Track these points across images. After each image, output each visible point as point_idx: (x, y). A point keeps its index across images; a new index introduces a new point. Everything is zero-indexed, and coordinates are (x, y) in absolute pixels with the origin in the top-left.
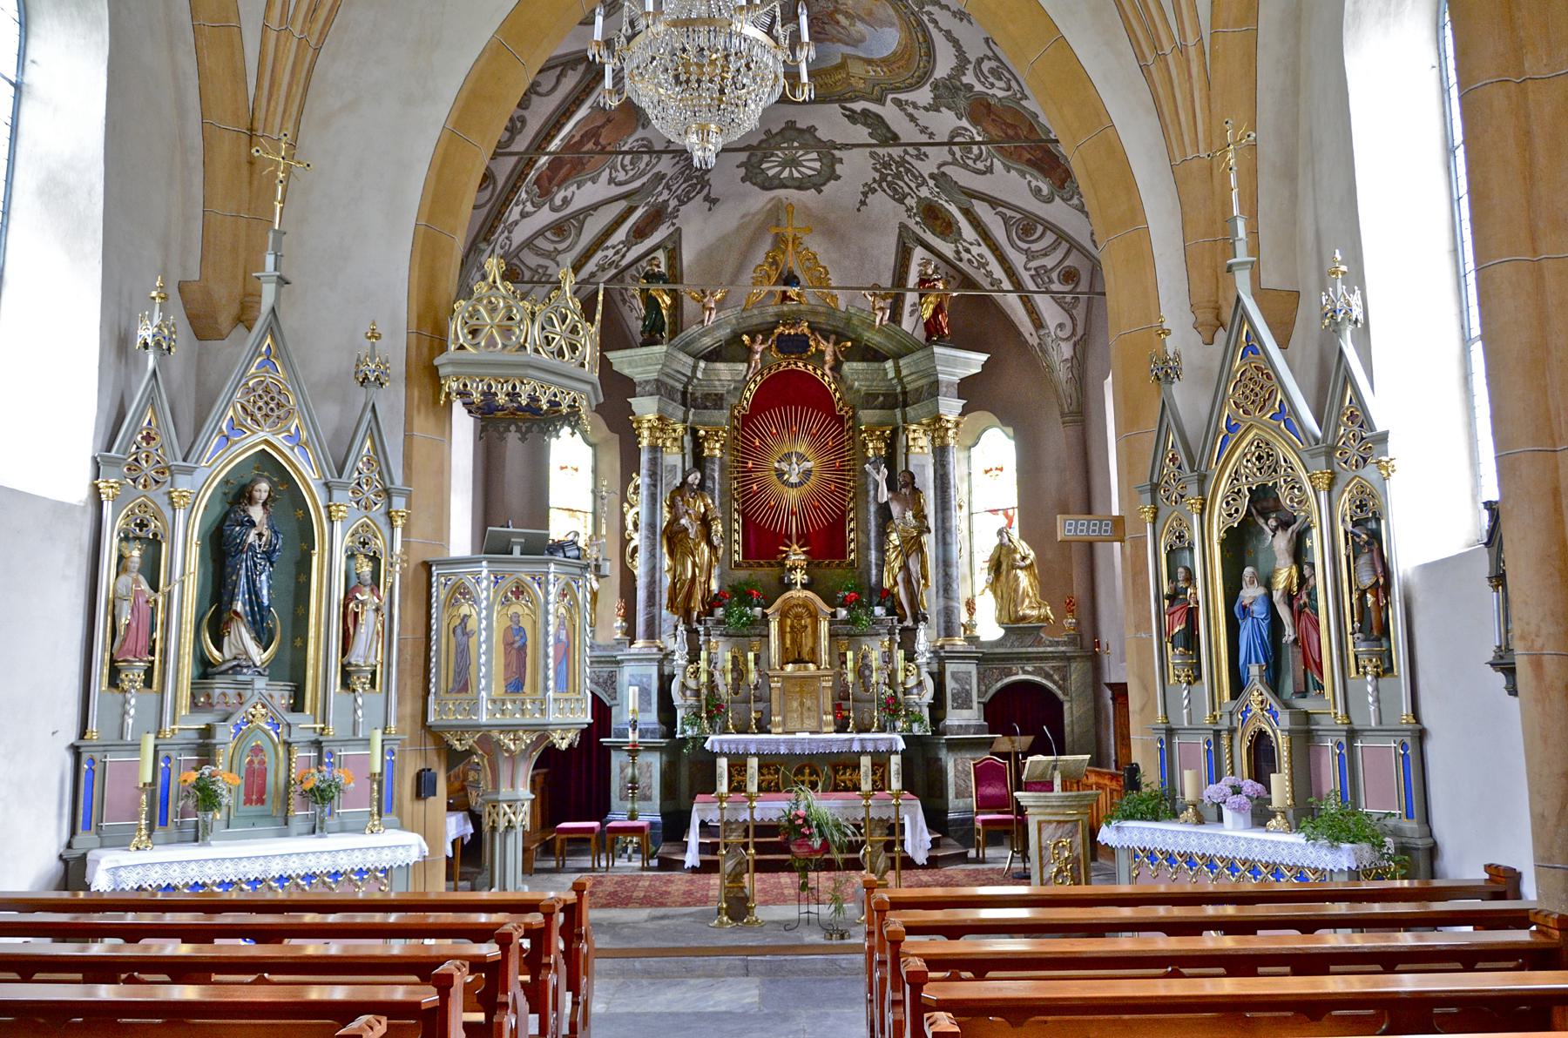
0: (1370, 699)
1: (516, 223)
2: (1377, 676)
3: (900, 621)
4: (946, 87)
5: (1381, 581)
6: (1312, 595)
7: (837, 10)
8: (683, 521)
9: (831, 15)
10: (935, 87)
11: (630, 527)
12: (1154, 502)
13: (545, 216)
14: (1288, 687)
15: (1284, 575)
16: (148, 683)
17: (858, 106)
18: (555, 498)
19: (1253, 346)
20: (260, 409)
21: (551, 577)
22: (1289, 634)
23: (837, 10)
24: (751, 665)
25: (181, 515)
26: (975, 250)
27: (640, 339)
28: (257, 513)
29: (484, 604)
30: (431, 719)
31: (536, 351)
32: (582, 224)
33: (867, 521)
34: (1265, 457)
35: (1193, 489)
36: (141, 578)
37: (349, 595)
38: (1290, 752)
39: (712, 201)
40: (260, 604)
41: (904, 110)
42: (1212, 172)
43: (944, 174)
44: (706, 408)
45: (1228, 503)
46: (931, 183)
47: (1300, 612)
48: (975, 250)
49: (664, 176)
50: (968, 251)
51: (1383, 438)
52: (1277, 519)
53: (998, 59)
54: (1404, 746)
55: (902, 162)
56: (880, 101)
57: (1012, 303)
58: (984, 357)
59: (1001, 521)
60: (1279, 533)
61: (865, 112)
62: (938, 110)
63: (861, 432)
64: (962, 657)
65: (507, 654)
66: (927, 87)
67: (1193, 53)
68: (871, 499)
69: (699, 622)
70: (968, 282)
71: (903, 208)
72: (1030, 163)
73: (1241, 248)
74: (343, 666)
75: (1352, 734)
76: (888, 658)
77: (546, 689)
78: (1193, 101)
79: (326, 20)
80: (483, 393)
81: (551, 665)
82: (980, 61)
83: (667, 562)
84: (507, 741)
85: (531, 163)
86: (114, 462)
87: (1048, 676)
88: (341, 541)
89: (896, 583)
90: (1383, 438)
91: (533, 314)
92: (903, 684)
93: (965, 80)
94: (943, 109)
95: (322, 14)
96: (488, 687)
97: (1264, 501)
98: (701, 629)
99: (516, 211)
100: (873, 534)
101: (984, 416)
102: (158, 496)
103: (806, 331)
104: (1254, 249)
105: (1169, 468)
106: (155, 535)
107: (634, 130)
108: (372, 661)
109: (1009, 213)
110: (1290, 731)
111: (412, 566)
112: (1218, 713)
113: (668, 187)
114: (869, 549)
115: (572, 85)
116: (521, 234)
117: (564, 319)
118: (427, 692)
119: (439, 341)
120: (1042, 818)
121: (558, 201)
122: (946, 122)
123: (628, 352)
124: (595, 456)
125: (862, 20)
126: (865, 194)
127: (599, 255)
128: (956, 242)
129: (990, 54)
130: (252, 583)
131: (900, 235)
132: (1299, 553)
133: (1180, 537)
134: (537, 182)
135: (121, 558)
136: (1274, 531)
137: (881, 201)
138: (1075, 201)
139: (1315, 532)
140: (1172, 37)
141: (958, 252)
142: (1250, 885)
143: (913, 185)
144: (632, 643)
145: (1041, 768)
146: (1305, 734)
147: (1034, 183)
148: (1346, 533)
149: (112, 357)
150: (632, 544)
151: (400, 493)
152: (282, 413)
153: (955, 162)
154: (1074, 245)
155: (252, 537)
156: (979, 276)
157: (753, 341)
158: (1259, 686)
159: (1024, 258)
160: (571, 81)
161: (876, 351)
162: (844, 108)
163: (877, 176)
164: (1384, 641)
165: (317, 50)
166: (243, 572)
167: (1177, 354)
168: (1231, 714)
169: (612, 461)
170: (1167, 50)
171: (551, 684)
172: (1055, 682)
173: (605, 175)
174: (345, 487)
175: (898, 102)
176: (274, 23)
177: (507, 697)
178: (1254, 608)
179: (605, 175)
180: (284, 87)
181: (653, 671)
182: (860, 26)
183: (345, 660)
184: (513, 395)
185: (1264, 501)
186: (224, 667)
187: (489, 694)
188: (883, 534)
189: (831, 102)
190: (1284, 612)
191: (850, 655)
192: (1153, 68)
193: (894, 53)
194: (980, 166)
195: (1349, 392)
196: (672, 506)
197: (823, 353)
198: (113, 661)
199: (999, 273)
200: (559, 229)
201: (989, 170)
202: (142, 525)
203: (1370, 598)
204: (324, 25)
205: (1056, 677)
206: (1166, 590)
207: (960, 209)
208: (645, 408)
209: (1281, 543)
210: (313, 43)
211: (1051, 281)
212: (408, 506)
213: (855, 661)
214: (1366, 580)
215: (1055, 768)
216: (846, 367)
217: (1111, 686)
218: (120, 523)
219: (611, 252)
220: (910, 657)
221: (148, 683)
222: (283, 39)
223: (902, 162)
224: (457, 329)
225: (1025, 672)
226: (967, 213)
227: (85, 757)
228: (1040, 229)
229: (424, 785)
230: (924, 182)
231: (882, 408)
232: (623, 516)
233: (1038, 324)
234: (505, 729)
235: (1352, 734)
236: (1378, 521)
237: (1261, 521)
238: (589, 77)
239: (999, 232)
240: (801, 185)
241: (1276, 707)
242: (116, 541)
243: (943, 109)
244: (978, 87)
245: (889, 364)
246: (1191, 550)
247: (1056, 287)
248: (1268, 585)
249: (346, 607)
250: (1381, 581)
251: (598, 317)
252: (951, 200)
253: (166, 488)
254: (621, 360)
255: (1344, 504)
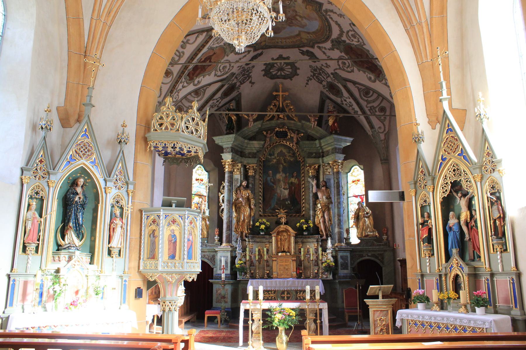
0: (499, 261)
1: (181, 90)
2: (501, 252)
3: (321, 237)
4: (336, 42)
5: (502, 216)
6: (476, 222)
7: (296, 15)
8: (241, 199)
9: (294, 17)
10: (332, 41)
11: (221, 201)
12: (415, 188)
13: (191, 88)
14: (467, 258)
15: (464, 214)
16: (37, 251)
17: (305, 49)
18: (194, 190)
19: (451, 130)
20: (81, 152)
21: (186, 216)
22: (467, 236)
23: (296, 15)
24: (265, 253)
25: (51, 190)
26: (348, 100)
27: (225, 132)
28: (79, 190)
29: (161, 225)
30: (141, 268)
31: (183, 131)
32: (205, 91)
33: (309, 200)
34: (456, 170)
35: (430, 183)
36: (36, 213)
37: (111, 222)
38: (469, 283)
39: (252, 83)
40: (79, 224)
41: (321, 50)
42: (433, 65)
43: (336, 73)
44: (250, 158)
45: (443, 188)
46: (332, 76)
47: (472, 228)
48: (348, 100)
49: (234, 74)
50: (345, 101)
51: (500, 162)
52: (461, 193)
53: (354, 31)
54: (513, 279)
55: (321, 69)
56: (313, 47)
57: (362, 119)
58: (352, 139)
59: (359, 200)
60: (462, 198)
61: (308, 51)
62: (333, 50)
63: (307, 167)
64: (344, 250)
65: (169, 244)
66: (329, 42)
67: (424, 25)
68: (311, 191)
69: (246, 237)
70: (346, 111)
71: (321, 86)
72: (367, 68)
73: (445, 92)
74: (109, 248)
75: (492, 275)
76: (317, 249)
77: (184, 259)
78: (425, 42)
79: (113, 16)
80: (163, 147)
81: (186, 249)
82: (348, 32)
83: (234, 214)
84: (169, 278)
85: (186, 68)
86: (29, 170)
87: (377, 257)
88: (110, 201)
89: (320, 222)
90: (500, 162)
91: (182, 118)
92: (321, 260)
93: (343, 39)
94: (335, 49)
95: (112, 14)
96: (162, 256)
97: (456, 186)
98: (247, 239)
99: (181, 85)
100: (311, 204)
101: (353, 162)
102: (43, 182)
103: (287, 130)
104: (449, 93)
105: (421, 176)
106: (42, 197)
107: (224, 57)
108: (119, 246)
109: (360, 87)
110: (468, 274)
111: (135, 210)
112: (440, 268)
113: (236, 78)
114: (310, 210)
115: (201, 40)
116: (182, 94)
117: (193, 119)
118: (140, 259)
119: (148, 127)
120: (375, 309)
121: (196, 82)
122: (336, 54)
123: (221, 137)
124: (209, 175)
125: (305, 18)
126: (308, 81)
127: (211, 102)
128: (341, 97)
129: (351, 29)
130: (76, 216)
131: (321, 95)
132: (470, 206)
133: (425, 201)
134: (188, 75)
135: (29, 205)
136: (460, 198)
137: (314, 83)
138: (384, 82)
139: (476, 198)
140: (416, 19)
141: (342, 101)
142: (454, 334)
143: (325, 77)
144: (221, 244)
145: (374, 290)
146: (475, 276)
147: (369, 76)
148: (488, 198)
149: (30, 132)
150: (222, 208)
151: (131, 184)
152: (89, 153)
153: (340, 69)
154: (384, 98)
155: (77, 199)
156: (350, 109)
157: (267, 133)
158: (456, 257)
159: (366, 103)
160: (202, 38)
161: (312, 137)
162: (300, 50)
163: (312, 74)
164: (503, 238)
165: (110, 27)
166: (73, 212)
167: (422, 132)
168: (446, 268)
169: (215, 175)
170: (415, 24)
171: (186, 257)
172: (379, 260)
173: (213, 73)
174: (111, 181)
175: (319, 48)
176: (95, 17)
177: (169, 261)
178: (454, 227)
179: (213, 73)
180: (98, 39)
181: (229, 255)
182: (305, 21)
183: (109, 246)
184: (174, 147)
185: (456, 186)
186: (65, 247)
187: (162, 260)
188: (315, 204)
189: (295, 48)
190: (465, 229)
191: (302, 249)
192: (410, 30)
193: (317, 30)
194: (349, 69)
195: (487, 145)
196: (236, 194)
197: (293, 137)
198: (24, 243)
199: (357, 108)
200: (197, 92)
201: (352, 71)
202: (37, 193)
203: (498, 222)
204: (112, 19)
205: (380, 258)
206: (420, 221)
207: (342, 85)
208: (227, 158)
209: (462, 203)
210: (108, 24)
211: (376, 111)
212: (134, 188)
213: (304, 252)
214: (496, 215)
215: (380, 290)
216: (301, 143)
217: (399, 260)
218: (29, 192)
219: (215, 101)
220: (324, 250)
221: (37, 251)
222: (98, 23)
223: (321, 69)
224: (155, 123)
225: (368, 256)
226: (345, 87)
227: (12, 279)
228: (371, 92)
229: (139, 293)
230: (329, 76)
231: (315, 158)
232: (219, 197)
233: (372, 127)
234: (168, 273)
235: (492, 275)
236: (499, 193)
237: (455, 194)
238: (207, 37)
239: (356, 94)
240: (285, 77)
241: (463, 266)
242: (27, 199)
243: (335, 49)
244: (348, 41)
245: (317, 142)
246: (429, 206)
247: (378, 113)
248: (459, 218)
249: (110, 226)
250: (502, 216)
251: (207, 120)
252: (339, 82)
253: (46, 180)
254: (219, 140)
255: (487, 186)
